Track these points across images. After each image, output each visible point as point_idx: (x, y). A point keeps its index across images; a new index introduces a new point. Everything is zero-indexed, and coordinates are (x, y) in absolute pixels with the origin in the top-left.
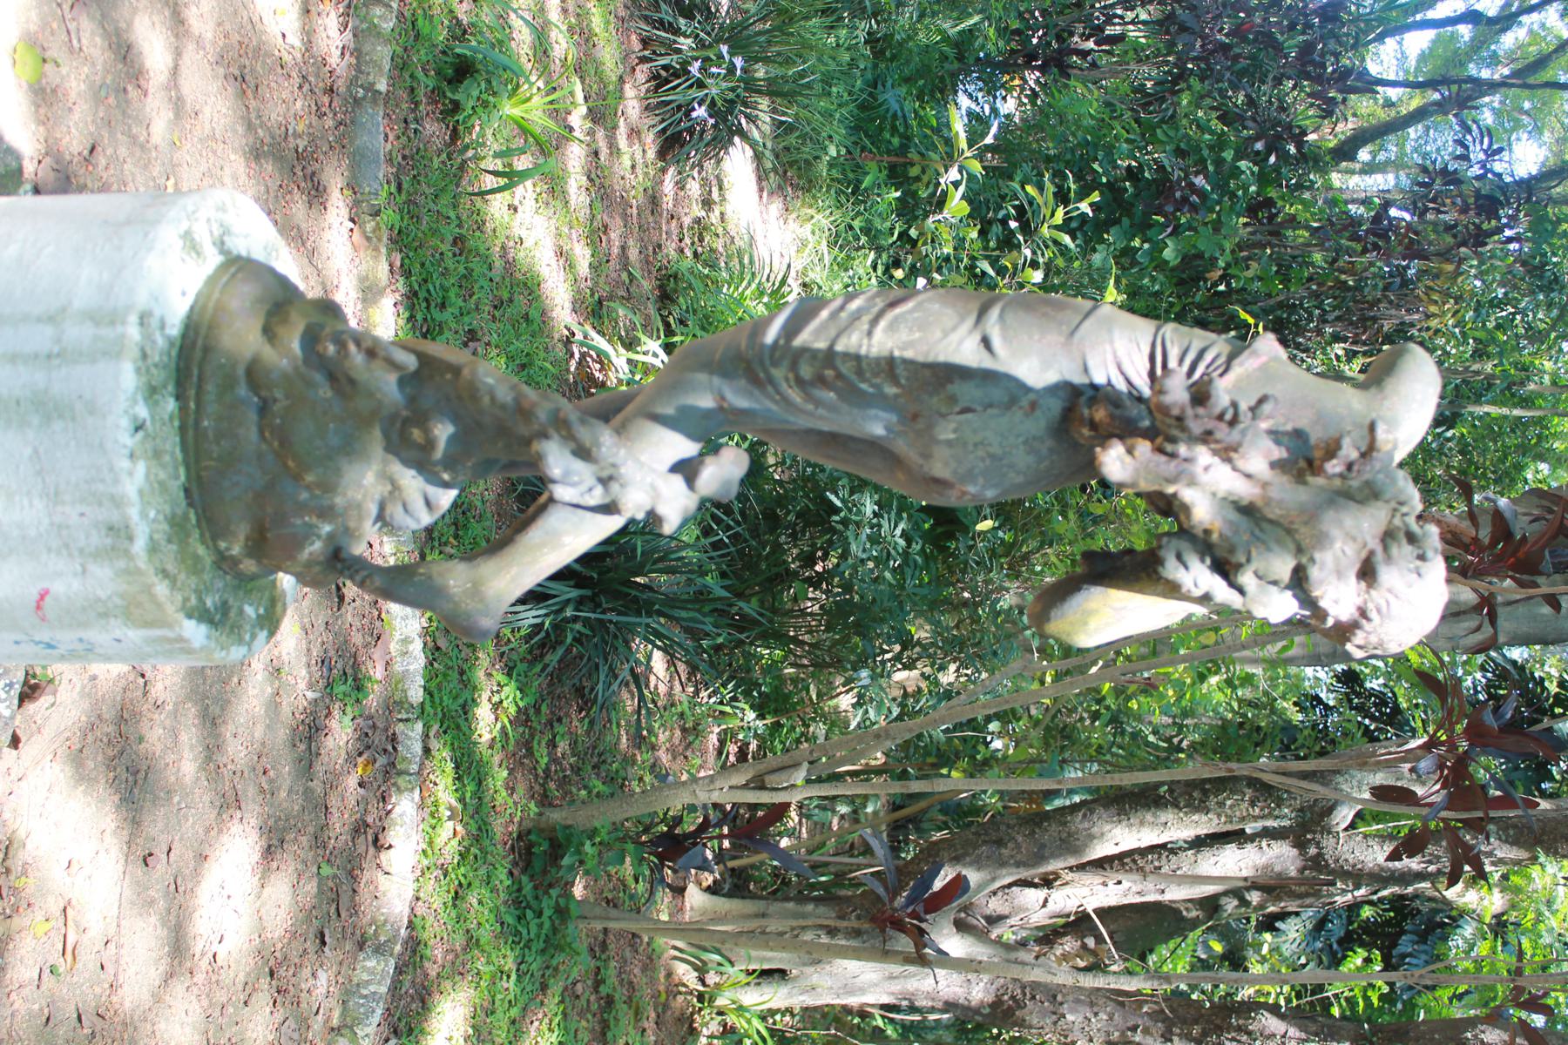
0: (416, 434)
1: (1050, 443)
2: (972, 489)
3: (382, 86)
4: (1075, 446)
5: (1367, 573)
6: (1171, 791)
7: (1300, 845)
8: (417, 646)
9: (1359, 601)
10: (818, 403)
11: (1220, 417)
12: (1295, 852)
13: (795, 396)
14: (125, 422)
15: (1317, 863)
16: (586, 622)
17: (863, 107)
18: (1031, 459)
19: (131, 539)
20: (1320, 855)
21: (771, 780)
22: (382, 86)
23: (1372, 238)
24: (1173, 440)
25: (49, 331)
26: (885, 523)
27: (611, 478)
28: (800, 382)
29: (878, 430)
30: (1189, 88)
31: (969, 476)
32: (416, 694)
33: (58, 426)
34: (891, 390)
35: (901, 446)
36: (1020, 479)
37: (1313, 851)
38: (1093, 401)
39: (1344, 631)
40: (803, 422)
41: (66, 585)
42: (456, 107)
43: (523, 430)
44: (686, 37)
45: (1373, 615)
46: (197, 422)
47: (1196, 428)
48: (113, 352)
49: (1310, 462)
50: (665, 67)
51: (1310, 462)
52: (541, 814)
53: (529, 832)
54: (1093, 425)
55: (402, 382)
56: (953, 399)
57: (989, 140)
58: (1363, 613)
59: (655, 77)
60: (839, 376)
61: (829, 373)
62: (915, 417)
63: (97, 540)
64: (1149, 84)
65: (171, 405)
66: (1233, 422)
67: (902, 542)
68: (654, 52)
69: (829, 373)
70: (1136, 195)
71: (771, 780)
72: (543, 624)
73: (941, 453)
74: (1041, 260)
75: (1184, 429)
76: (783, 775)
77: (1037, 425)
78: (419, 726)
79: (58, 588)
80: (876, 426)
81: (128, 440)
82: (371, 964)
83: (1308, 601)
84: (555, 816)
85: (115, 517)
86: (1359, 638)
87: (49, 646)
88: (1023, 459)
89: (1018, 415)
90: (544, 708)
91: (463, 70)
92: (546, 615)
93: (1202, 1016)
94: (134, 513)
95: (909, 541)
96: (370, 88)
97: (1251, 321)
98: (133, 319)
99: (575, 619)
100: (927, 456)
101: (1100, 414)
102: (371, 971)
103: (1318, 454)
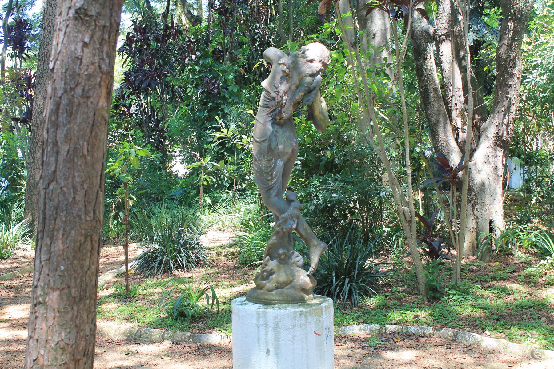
0: (283, 257)
1: (284, 128)
2: (294, 144)
3: (189, 334)
4: (285, 122)
5: (311, 61)
6: (422, 87)
7: (442, 41)
8: (362, 326)
9: (318, 62)
10: (276, 175)
11: (278, 95)
12: (444, 43)
13: (275, 180)
14: (279, 311)
15: (447, 35)
16: (358, 280)
17: (181, 203)
18: (288, 132)
19: (303, 311)
20: (444, 35)
21: (408, 218)
22: (189, 334)
23: (228, 15)
24: (282, 103)
25: (261, 327)
26: (331, 188)
27: (291, 216)
28: (272, 179)
29: (282, 163)
30: (170, 81)
31: (291, 144)
32: (377, 327)
33: (280, 325)
34: (273, 160)
35: (285, 158)
36: (292, 134)
37: (443, 37)
38: (275, 119)
39: (325, 65)
40: (280, 178)
41: (312, 327)
42: (193, 317)
43: (281, 233)
44: (163, 258)
45: (320, 59)
46: (280, 301)
47: (280, 99)
48: (265, 314)
49: (287, 76)
50: (174, 266)
51: (287, 76)
52: (422, 294)
53: (427, 298)
54: (280, 119)
55: (272, 260)
56: (275, 148)
57: (198, 154)
58: (320, 61)
59: (177, 269)
60: (271, 171)
61: (270, 173)
62: (279, 155)
63: (303, 318)
64: (168, 97)
65: (276, 305)
66: (279, 92)
67: (337, 183)
68: (168, 269)
69: (270, 173)
70: (213, 102)
71: (408, 218)
72: (359, 293)
73: (286, 150)
74: (239, 136)
75: (280, 102)
76: (406, 214)
77: (280, 131)
78: (387, 326)
79: (314, 330)
80: (280, 163)
81: (283, 310)
82: (460, 338)
83: (318, 73)
84: (422, 289)
85: (298, 314)
86: (326, 61)
87: (327, 337)
88: (288, 134)
89: (278, 135)
90: (387, 294)
91: (182, 315)
92: (355, 292)
93: (501, 74)
94: (297, 310)
95: (336, 180)
96: (189, 337)
97: (259, 63)
98: (259, 310)
99: (357, 283)
100: (287, 153)
101: (278, 118)
102: (462, 337)
103: (285, 74)
